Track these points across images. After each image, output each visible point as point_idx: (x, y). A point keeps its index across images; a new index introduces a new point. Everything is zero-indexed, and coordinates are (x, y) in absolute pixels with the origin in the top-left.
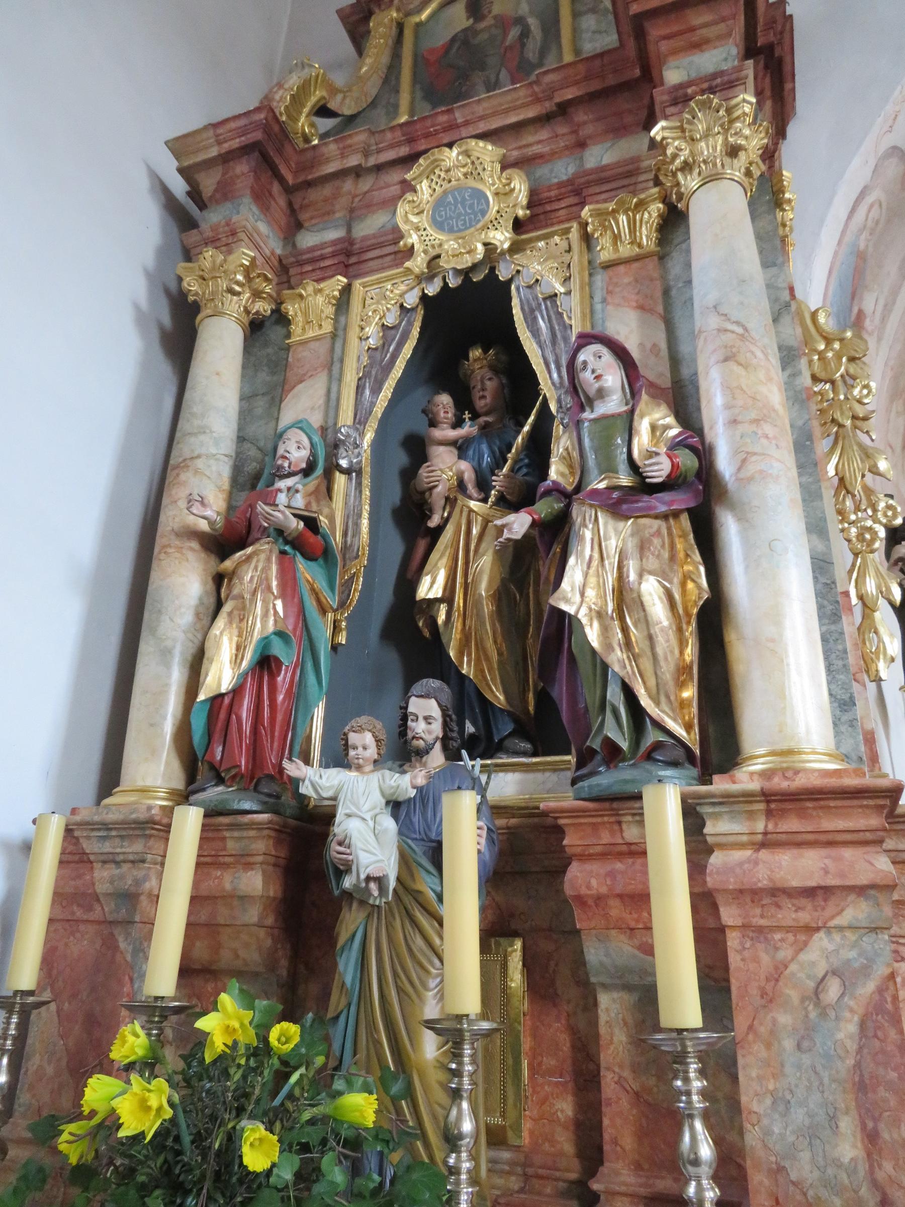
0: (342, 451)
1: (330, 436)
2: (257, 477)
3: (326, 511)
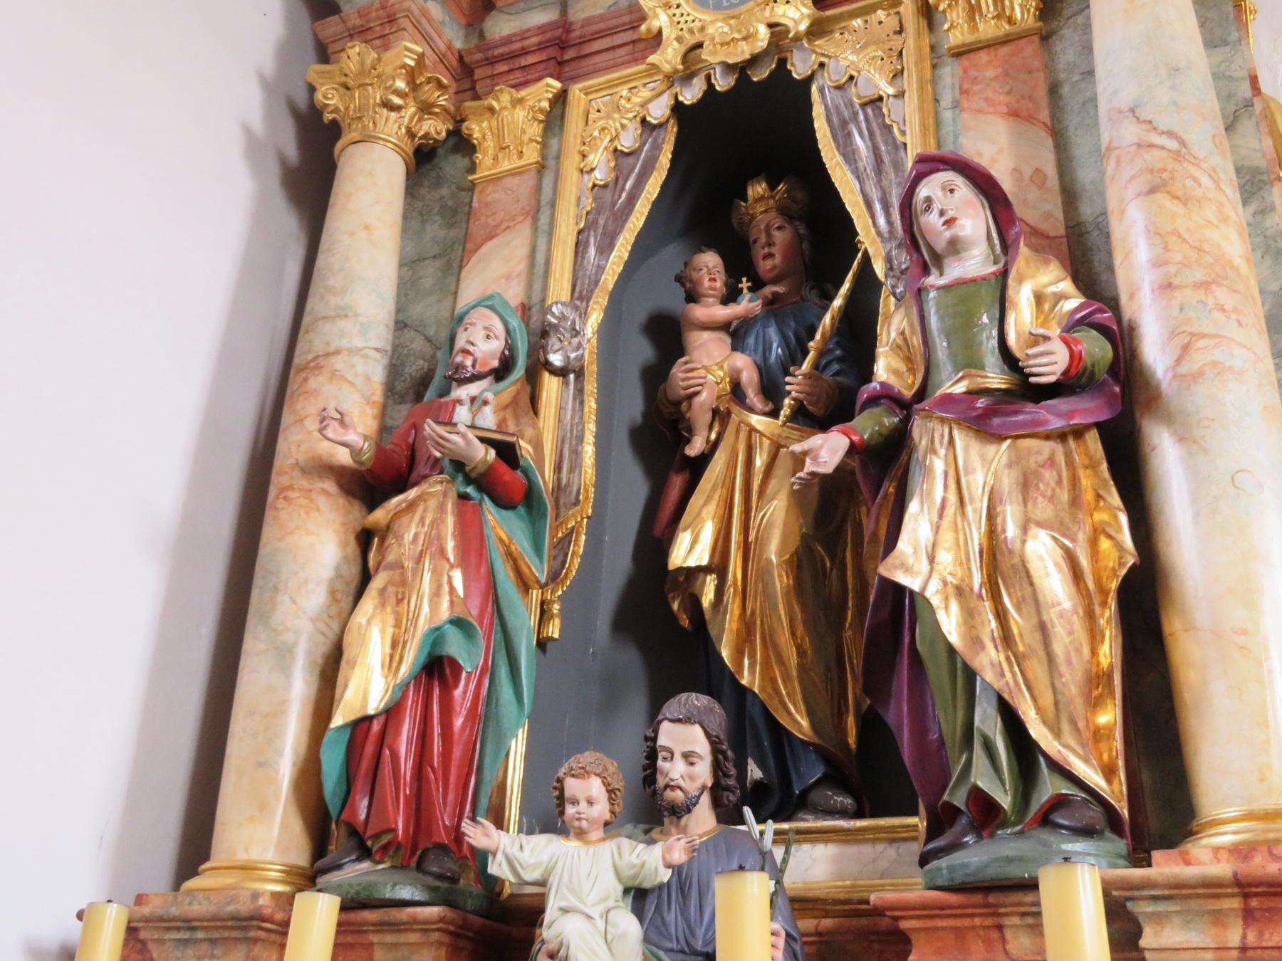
0: (553, 341)
1: (535, 319)
3: (529, 432)
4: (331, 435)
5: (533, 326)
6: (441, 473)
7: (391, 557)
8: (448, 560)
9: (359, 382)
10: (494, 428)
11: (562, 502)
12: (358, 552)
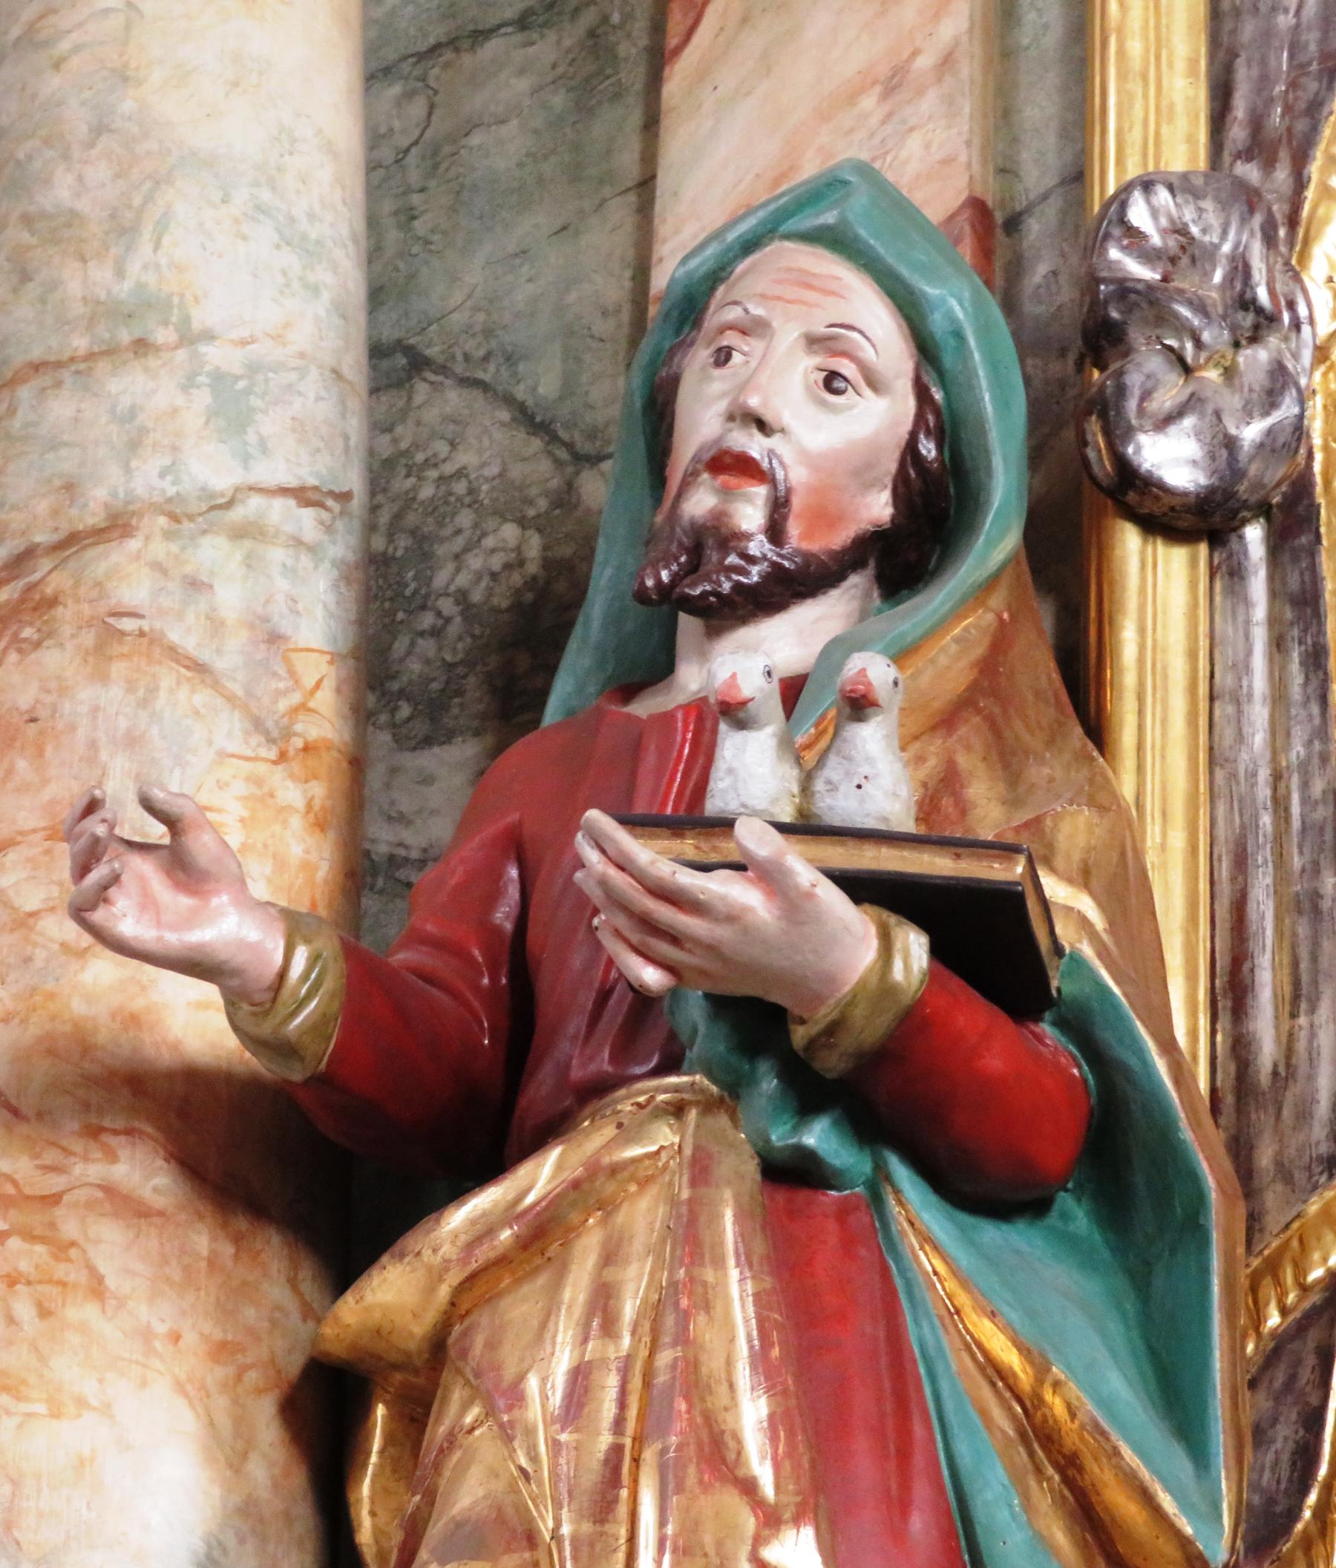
0: (1147, 373)
1: (1044, 267)
2: (530, 632)
3: (1076, 830)
4: (129, 925)
5: (1033, 309)
6: (671, 1064)
7: (469, 1492)
8: (748, 1487)
9: (229, 658)
10: (908, 825)
11: (1265, 1157)
12: (299, 1479)
